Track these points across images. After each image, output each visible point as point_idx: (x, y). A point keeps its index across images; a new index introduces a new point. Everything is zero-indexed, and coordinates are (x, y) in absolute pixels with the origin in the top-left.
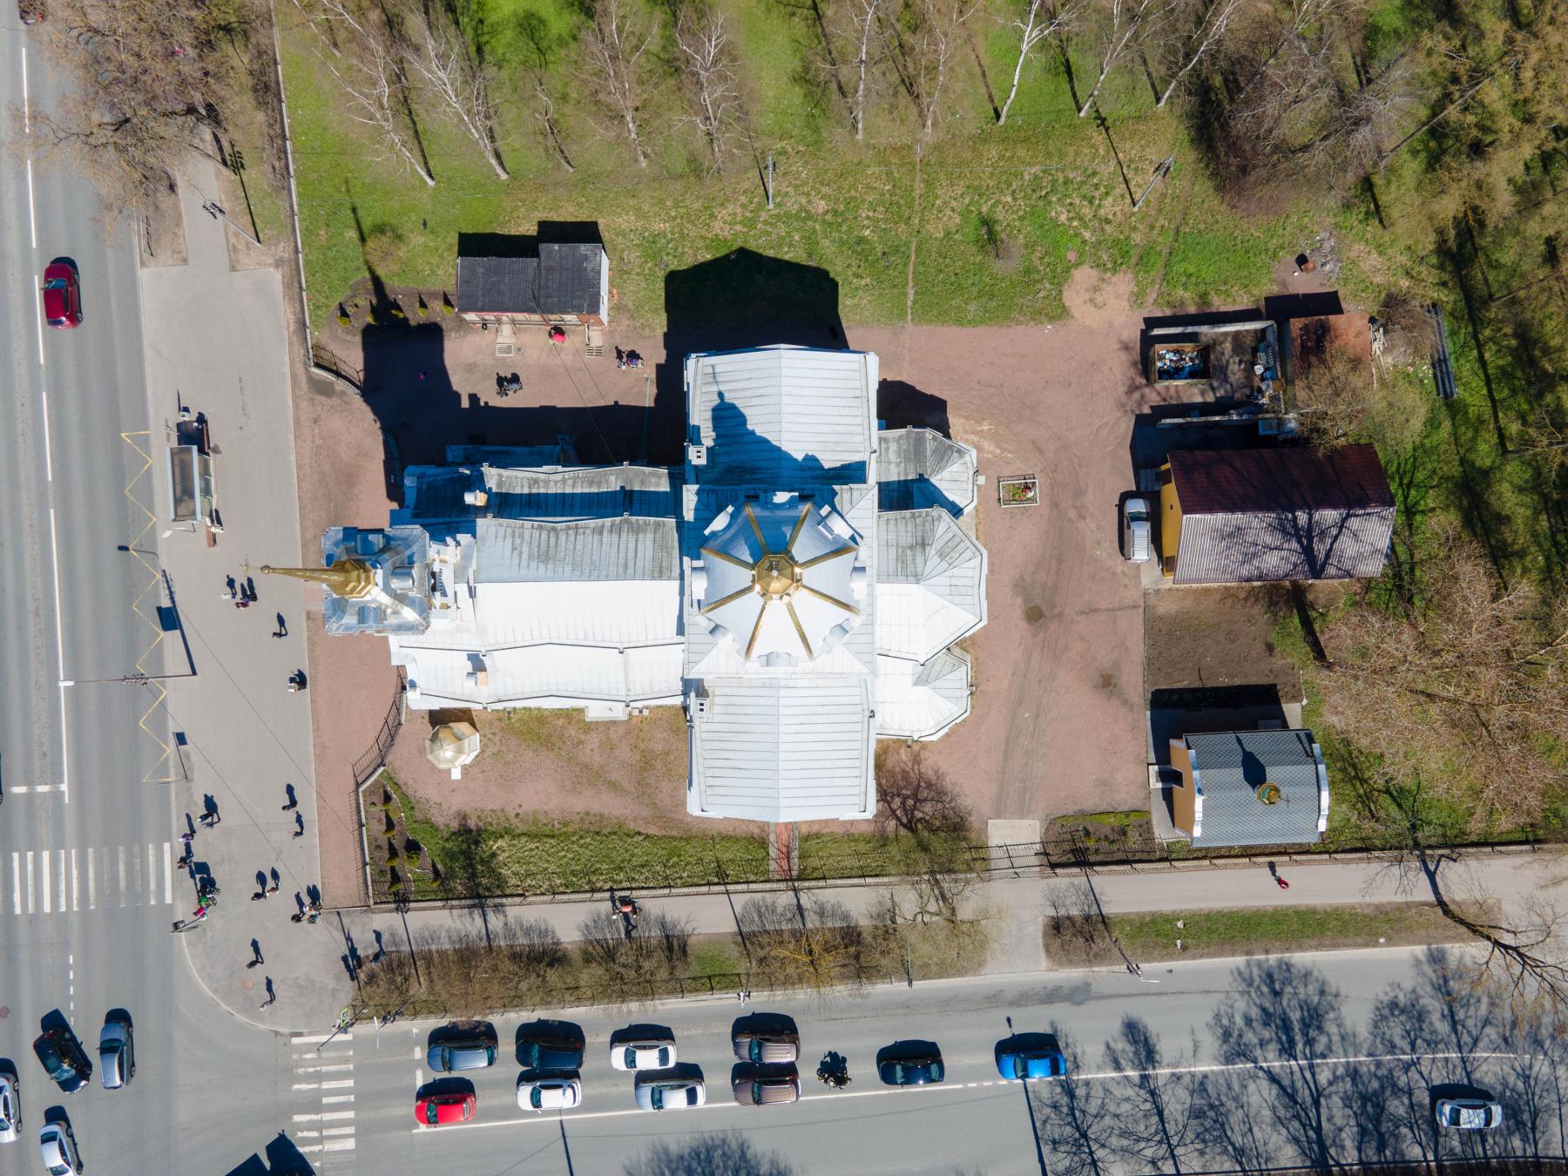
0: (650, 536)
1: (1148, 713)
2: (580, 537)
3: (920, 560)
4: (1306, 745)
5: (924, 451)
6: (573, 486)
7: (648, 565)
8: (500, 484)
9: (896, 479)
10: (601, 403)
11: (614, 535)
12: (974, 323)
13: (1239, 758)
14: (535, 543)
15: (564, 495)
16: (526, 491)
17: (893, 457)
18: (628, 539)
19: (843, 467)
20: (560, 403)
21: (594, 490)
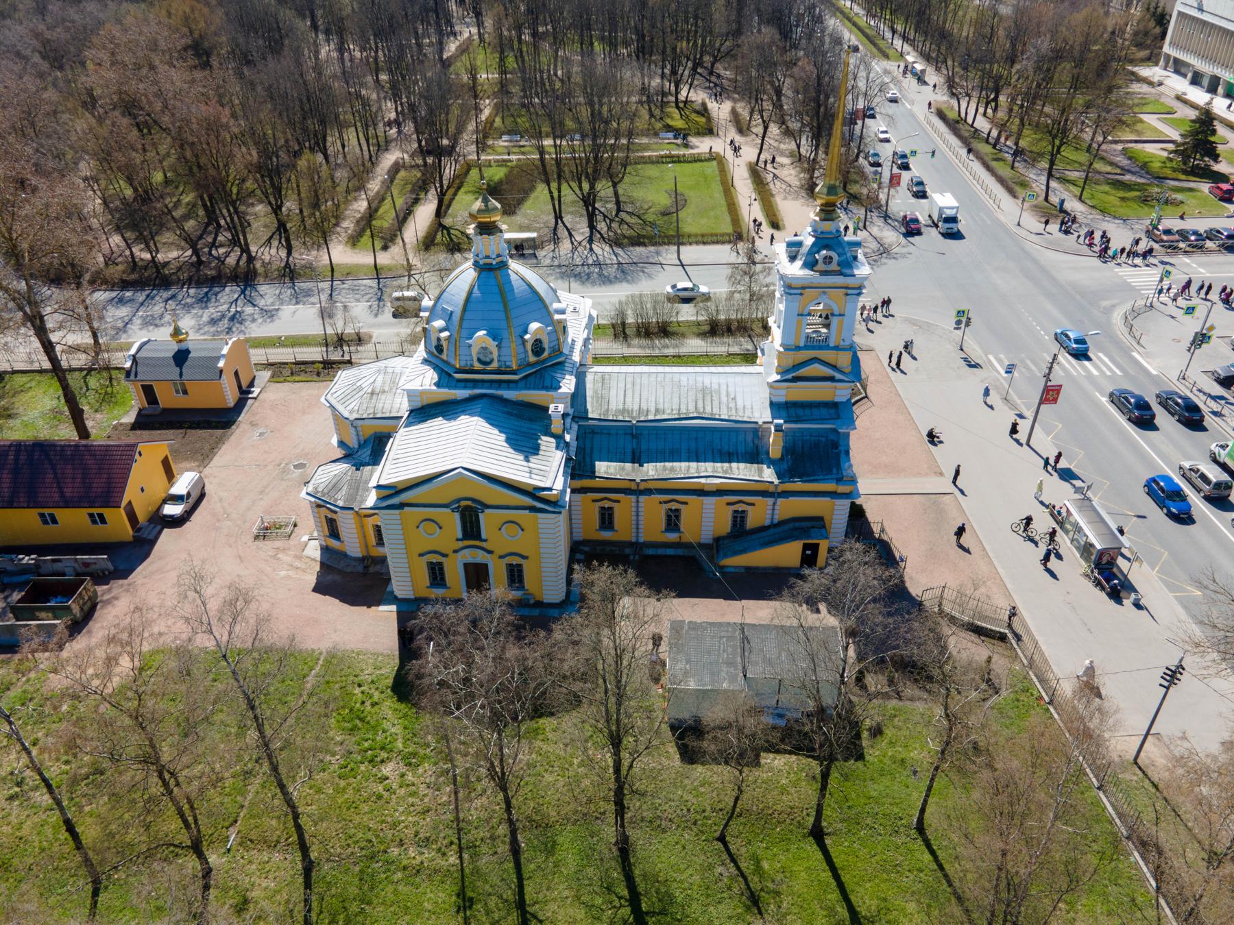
0: (613, 406)
2: (675, 407)
4: (134, 369)
6: (689, 467)
7: (614, 384)
8: (760, 472)
11: (645, 408)
14: (716, 403)
15: (698, 461)
16: (734, 465)
18: (633, 404)
20: (721, 600)
21: (669, 465)
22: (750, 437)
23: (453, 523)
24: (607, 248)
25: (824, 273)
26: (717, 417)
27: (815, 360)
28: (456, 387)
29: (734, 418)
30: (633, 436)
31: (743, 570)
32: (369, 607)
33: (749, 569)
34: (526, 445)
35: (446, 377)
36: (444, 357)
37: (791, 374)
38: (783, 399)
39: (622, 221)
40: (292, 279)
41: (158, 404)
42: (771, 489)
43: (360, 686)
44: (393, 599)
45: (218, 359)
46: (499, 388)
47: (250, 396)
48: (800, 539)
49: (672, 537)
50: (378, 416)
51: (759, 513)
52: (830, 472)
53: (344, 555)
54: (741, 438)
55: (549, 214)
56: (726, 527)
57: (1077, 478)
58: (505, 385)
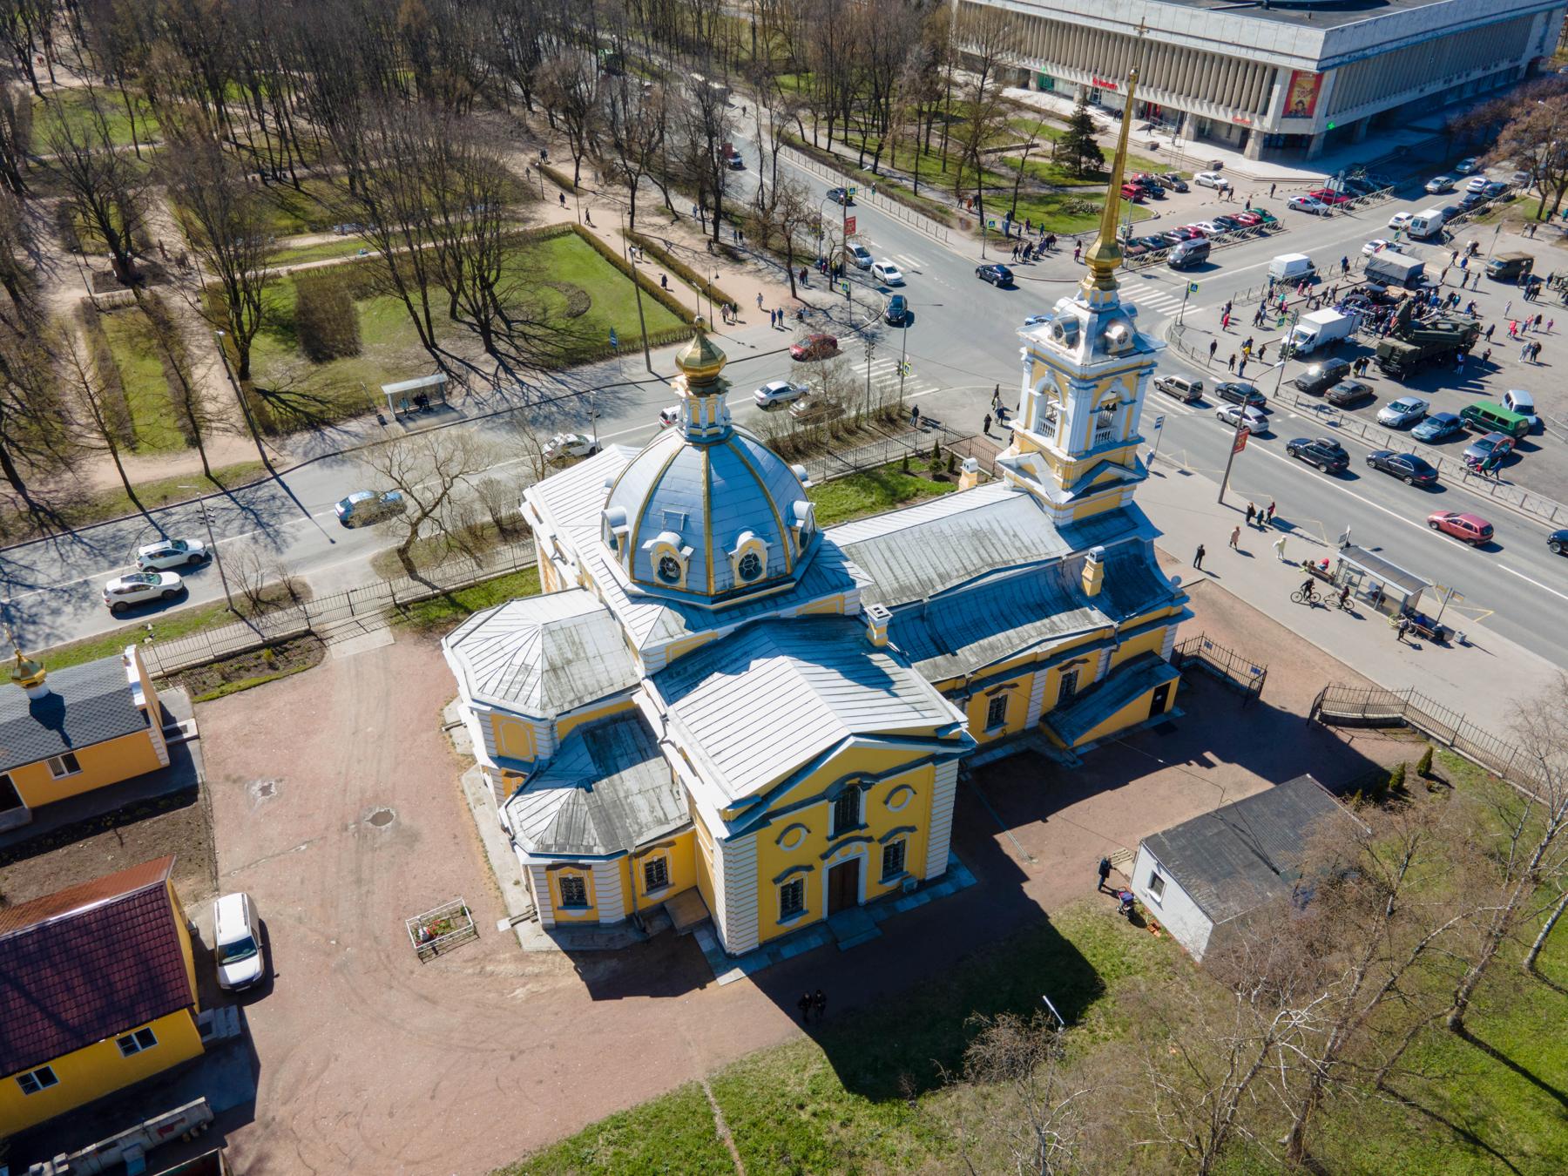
1: (199, 781)
3: (553, 652)
5: (597, 825)
8: (1087, 617)
9: (624, 774)
10: (1064, 813)
11: (925, 578)
12: (593, 1132)
13: (68, 718)
14: (999, 546)
15: (1013, 627)
16: (1055, 618)
17: (640, 802)
19: (696, 684)
20: (1107, 795)
21: (984, 642)
22: (1051, 579)
23: (825, 814)
24: (541, 376)
25: (1122, 354)
26: (1013, 564)
27: (1104, 464)
28: (720, 624)
29: (1030, 560)
30: (922, 618)
31: (1096, 746)
32: (702, 987)
33: (1099, 741)
34: (881, 681)
35: (694, 616)
36: (681, 584)
37: (1084, 487)
38: (1069, 521)
39: (524, 336)
40: (64, 527)
41: (20, 803)
42: (1109, 634)
43: (801, 1107)
44: (731, 961)
45: (128, 691)
46: (777, 606)
47: (186, 736)
48: (1150, 686)
49: (995, 733)
50: (587, 700)
51: (1090, 670)
52: (1155, 595)
53: (596, 925)
54: (1042, 582)
55: (413, 344)
56: (1054, 699)
57: (1294, 527)
58: (781, 600)
